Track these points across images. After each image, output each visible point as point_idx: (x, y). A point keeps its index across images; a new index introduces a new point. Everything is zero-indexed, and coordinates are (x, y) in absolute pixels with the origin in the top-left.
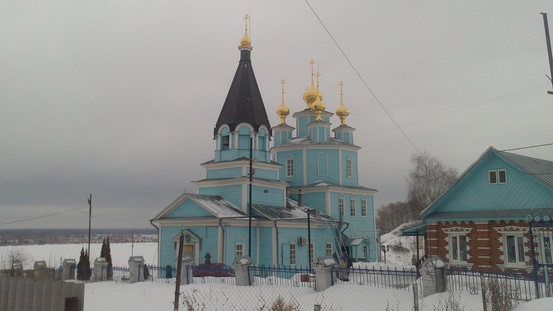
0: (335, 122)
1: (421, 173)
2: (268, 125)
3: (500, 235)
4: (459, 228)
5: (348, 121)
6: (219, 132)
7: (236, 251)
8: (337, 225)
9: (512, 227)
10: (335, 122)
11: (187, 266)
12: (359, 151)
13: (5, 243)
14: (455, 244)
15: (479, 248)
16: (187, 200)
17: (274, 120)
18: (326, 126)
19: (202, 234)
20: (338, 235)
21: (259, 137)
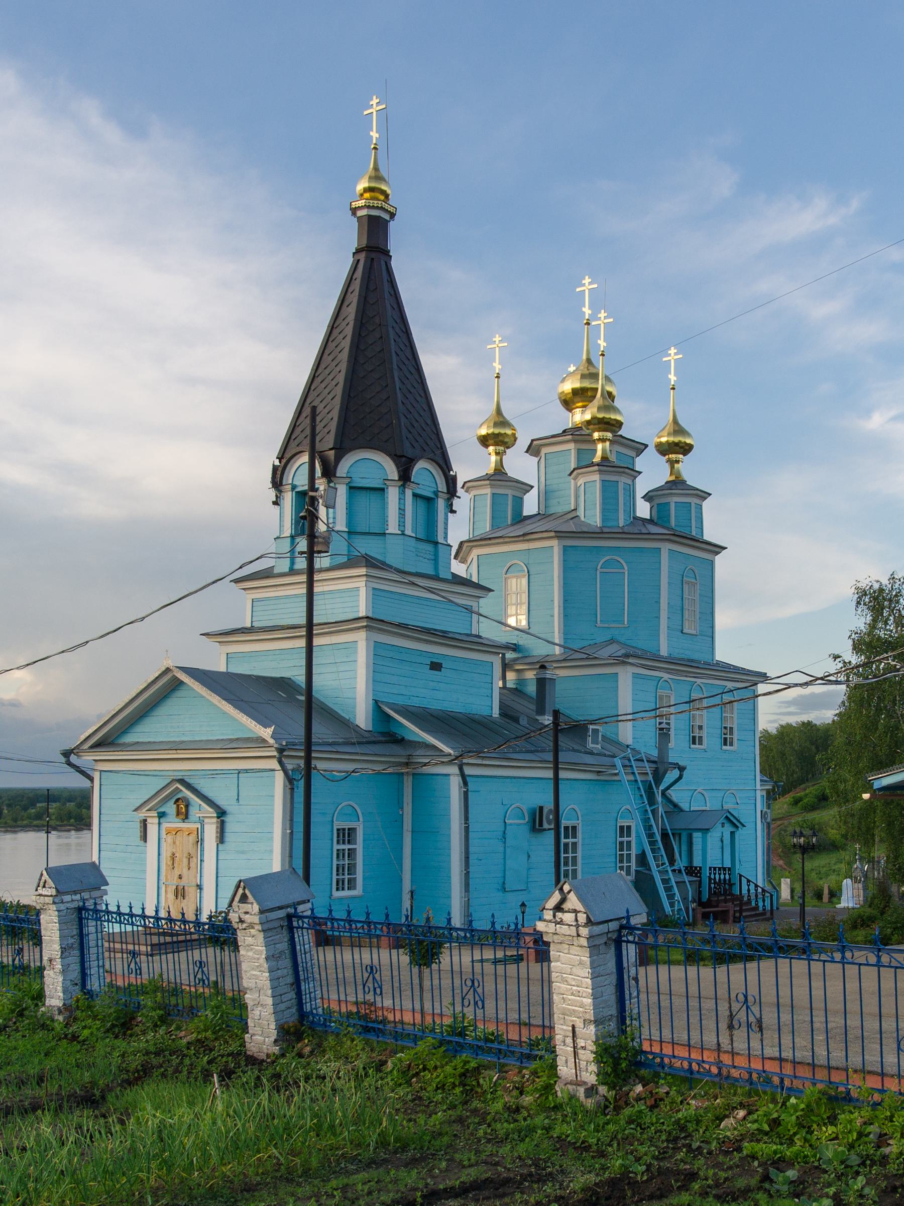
0: (652, 472)
2: (444, 464)
5: (691, 470)
6: (288, 479)
7: (336, 847)
10: (652, 472)
11: (80, 910)
12: (719, 560)
13: (14, 825)
16: (176, 684)
17: (470, 463)
19: (222, 794)
20: (652, 801)
21: (415, 495)
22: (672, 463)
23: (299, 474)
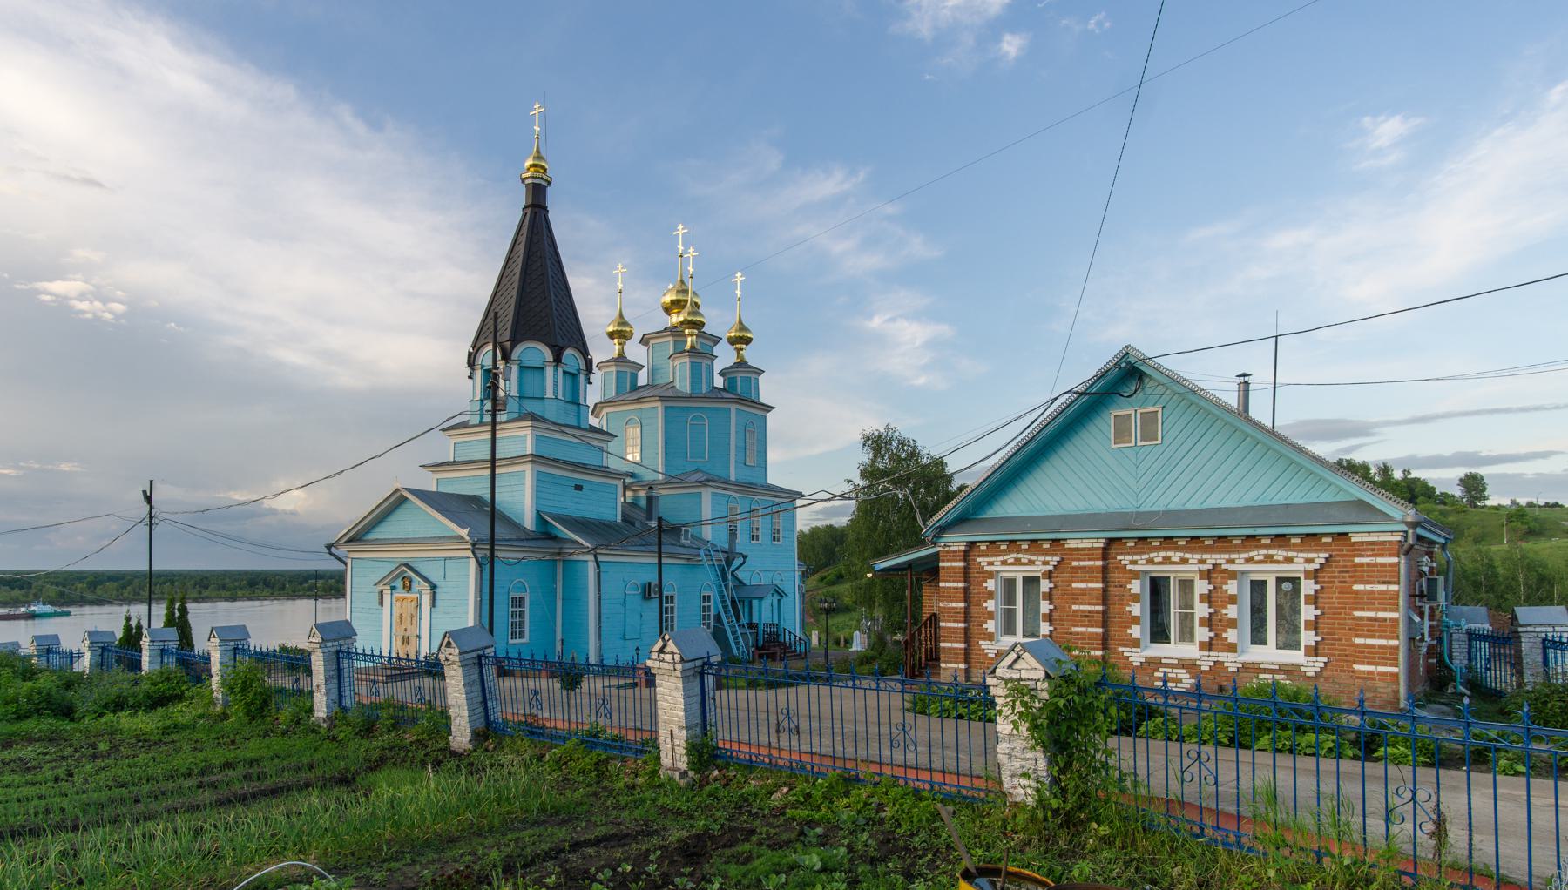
0: (725, 357)
1: (885, 463)
2: (584, 351)
3: (991, 575)
4: (1025, 558)
5: (751, 355)
6: (479, 361)
8: (722, 556)
9: (1170, 554)
10: (725, 357)
11: (338, 652)
14: (1258, 611)
15: (1075, 607)
16: (403, 500)
18: (706, 362)
19: (434, 574)
20: (725, 578)
22: (738, 350)
23: (486, 358)
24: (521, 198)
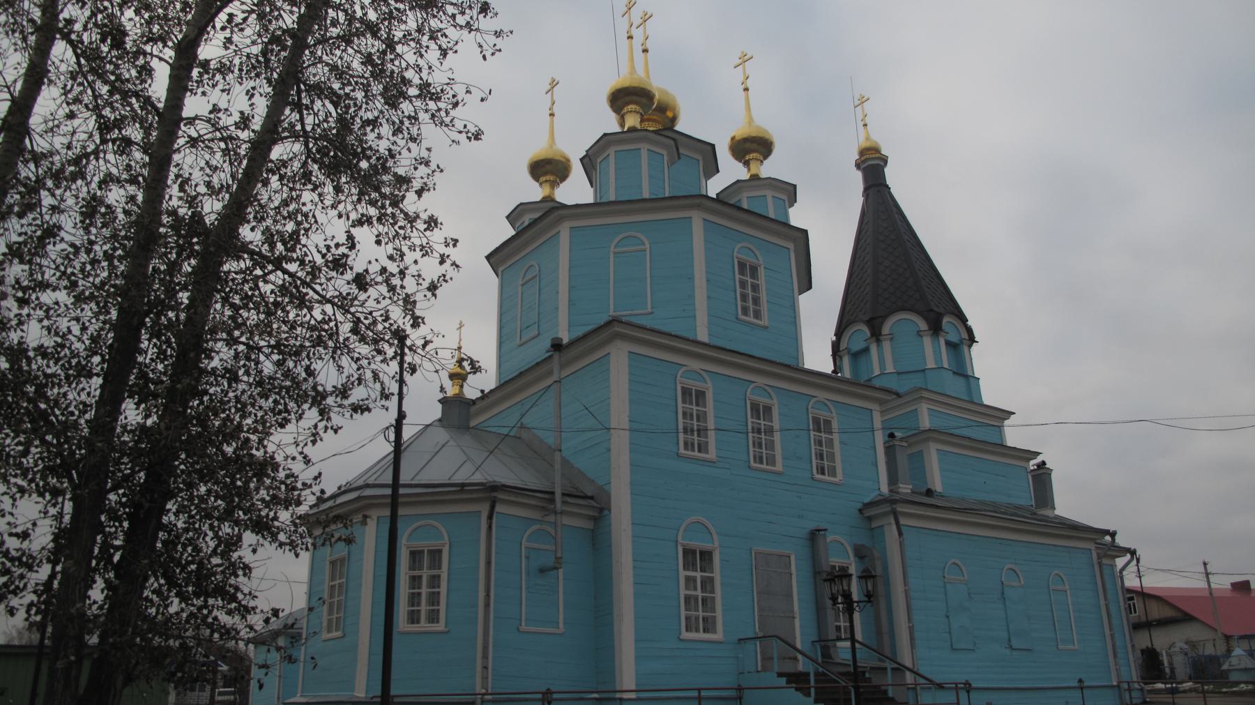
5: (769, 169)
24: (857, 180)
